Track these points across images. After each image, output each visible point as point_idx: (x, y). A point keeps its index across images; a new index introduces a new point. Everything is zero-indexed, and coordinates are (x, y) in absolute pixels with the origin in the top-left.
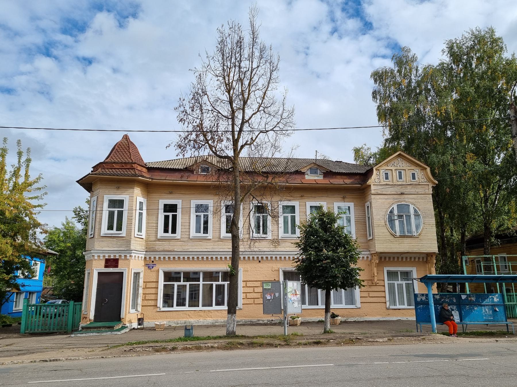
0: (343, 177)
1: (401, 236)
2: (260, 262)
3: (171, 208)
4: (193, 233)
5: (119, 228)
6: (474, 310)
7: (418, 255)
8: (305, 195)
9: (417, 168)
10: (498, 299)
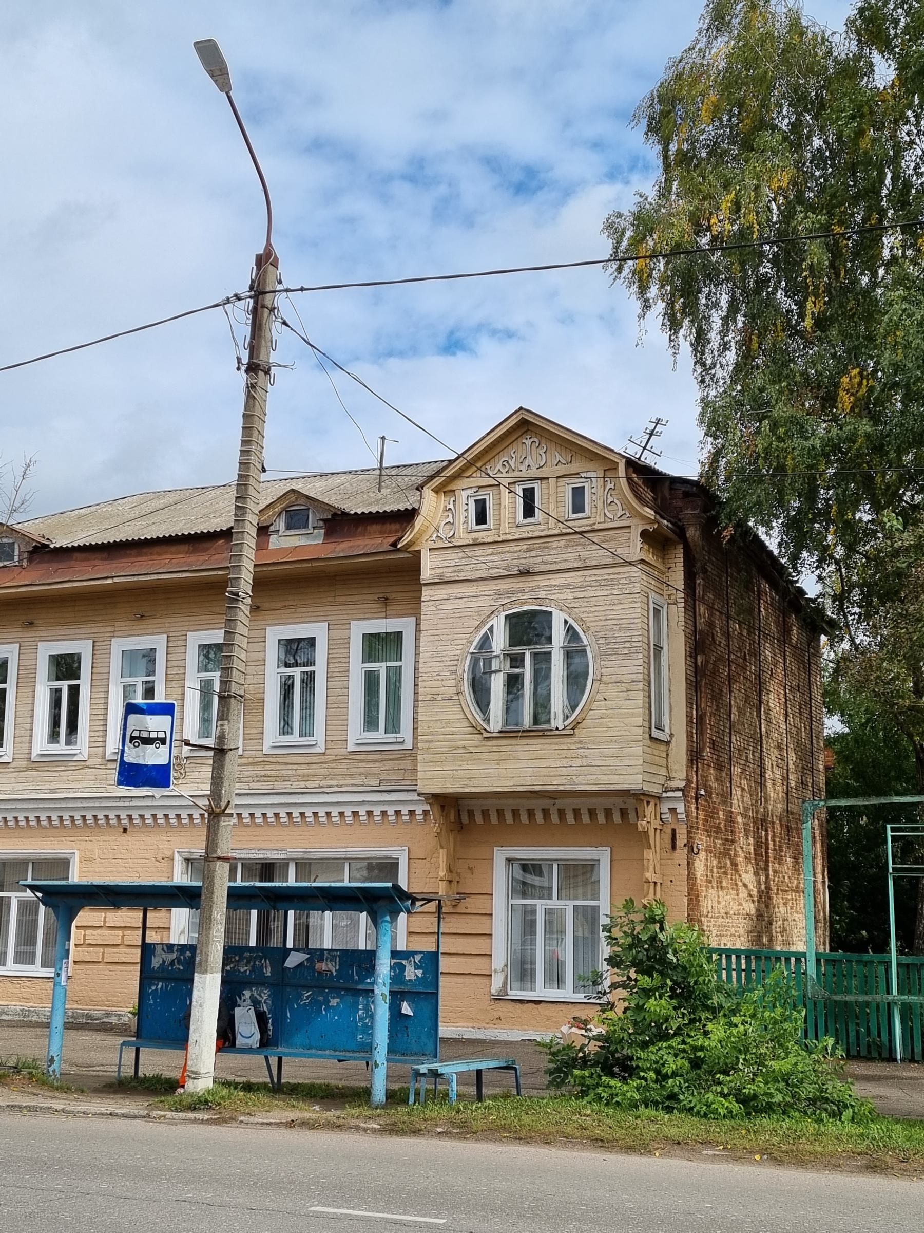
0: (388, 527)
1: (504, 734)
2: (125, 830)
3: (66, 667)
4: (41, 744)
5: (393, 725)
6: (328, 1008)
7: (546, 803)
8: (266, 605)
9: (592, 466)
10: (419, 973)
